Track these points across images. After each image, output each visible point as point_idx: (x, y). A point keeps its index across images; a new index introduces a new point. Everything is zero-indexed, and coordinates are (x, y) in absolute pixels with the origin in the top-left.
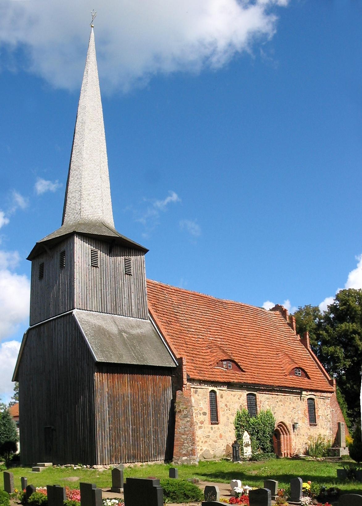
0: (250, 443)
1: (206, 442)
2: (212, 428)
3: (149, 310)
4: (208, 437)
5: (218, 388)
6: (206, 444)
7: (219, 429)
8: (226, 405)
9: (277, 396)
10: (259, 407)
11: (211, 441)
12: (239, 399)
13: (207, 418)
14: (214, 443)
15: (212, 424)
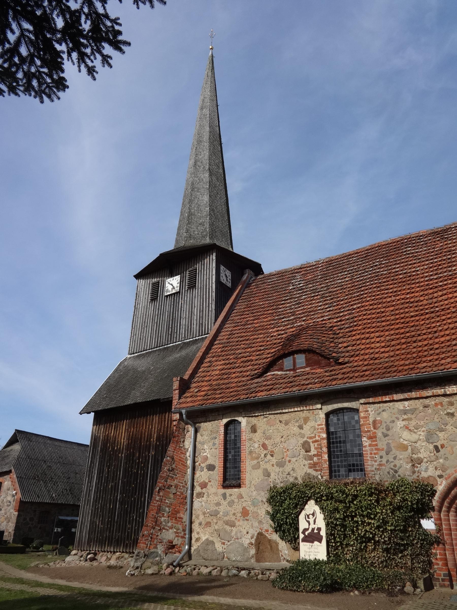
0: (323, 533)
1: (208, 524)
2: (224, 496)
3: (216, 320)
4: (215, 514)
5: (362, 401)
6: (209, 529)
7: (240, 497)
8: (264, 446)
9: (446, 400)
10: (372, 438)
11: (220, 523)
12: (301, 427)
13: (218, 474)
14: (228, 528)
15: (225, 487)
